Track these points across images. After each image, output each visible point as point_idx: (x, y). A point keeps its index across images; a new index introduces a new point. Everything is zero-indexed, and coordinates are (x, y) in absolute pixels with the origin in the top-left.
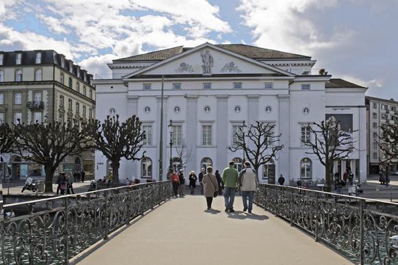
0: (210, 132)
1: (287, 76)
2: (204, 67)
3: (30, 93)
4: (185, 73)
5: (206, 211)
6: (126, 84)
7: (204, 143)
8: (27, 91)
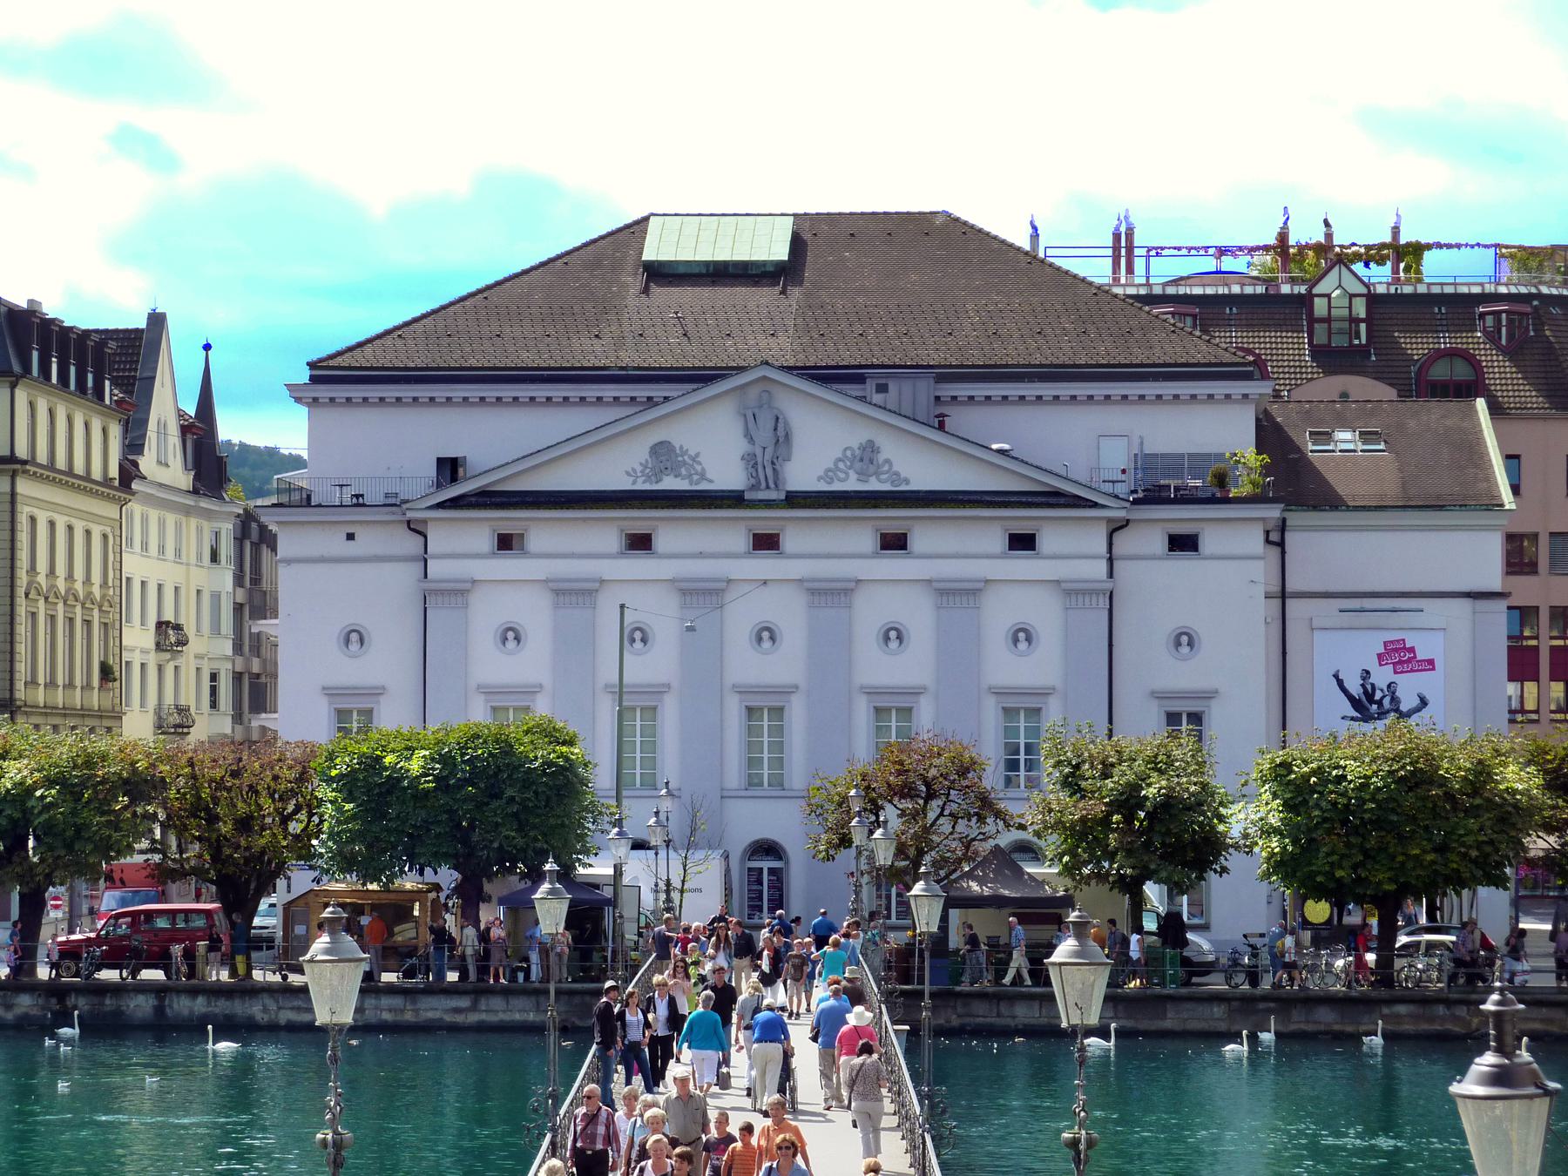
0: (778, 731)
1: (1095, 505)
2: (751, 461)
4: (670, 483)
5: (1338, 671)
6: (417, 529)
7: (753, 782)
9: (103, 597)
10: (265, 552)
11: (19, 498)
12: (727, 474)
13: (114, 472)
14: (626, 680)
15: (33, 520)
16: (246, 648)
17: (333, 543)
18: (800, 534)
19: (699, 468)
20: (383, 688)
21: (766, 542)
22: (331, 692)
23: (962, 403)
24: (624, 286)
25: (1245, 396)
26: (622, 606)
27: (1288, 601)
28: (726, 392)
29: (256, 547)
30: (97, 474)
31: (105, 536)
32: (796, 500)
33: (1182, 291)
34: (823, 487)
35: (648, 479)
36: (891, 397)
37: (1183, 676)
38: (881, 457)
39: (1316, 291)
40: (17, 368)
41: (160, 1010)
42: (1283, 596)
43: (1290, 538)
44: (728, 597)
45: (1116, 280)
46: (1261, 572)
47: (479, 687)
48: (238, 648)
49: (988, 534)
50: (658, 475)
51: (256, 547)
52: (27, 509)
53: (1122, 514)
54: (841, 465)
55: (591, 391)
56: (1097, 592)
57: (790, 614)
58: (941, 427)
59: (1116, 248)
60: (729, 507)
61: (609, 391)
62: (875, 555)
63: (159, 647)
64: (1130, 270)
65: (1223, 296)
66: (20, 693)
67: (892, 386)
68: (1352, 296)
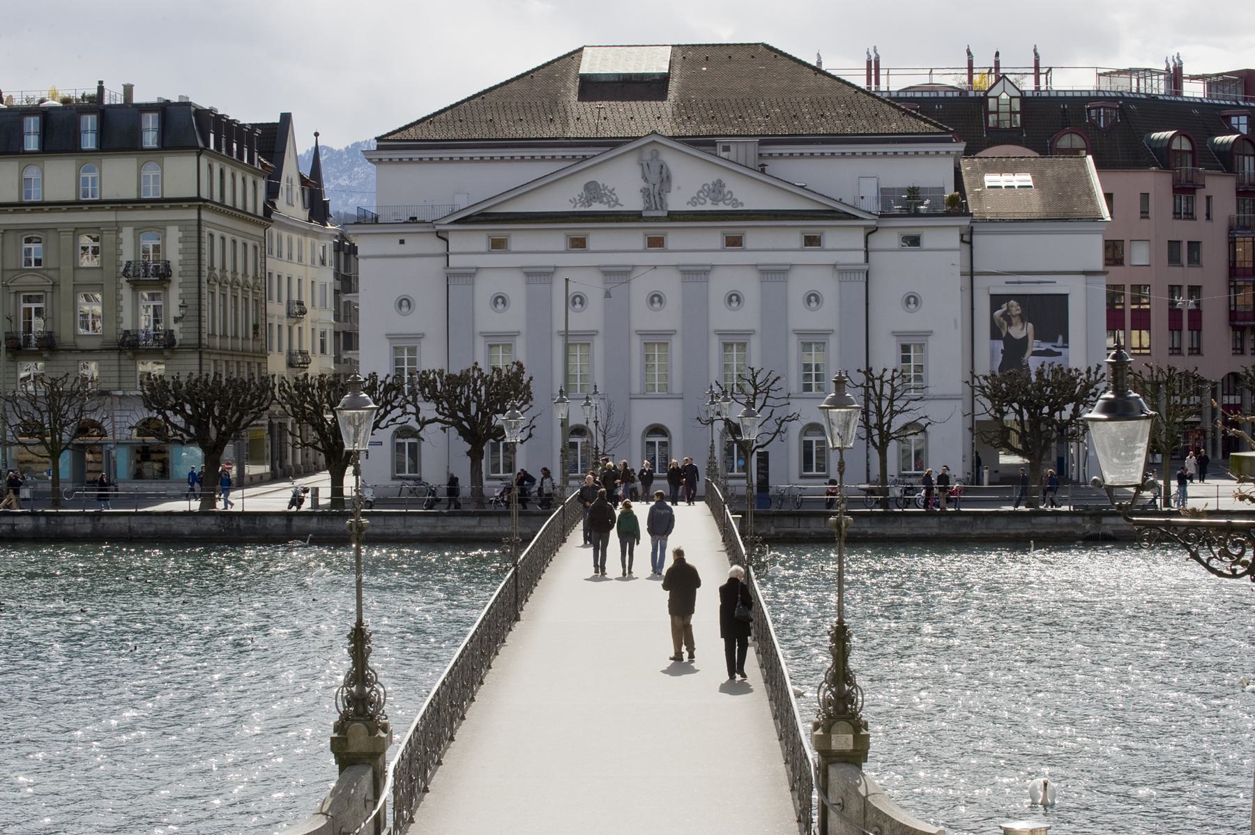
1: (856, 218)
2: (646, 193)
3: (127, 234)
4: (597, 207)
5: (664, 672)
6: (442, 236)
8: (117, 227)
9: (254, 284)
11: (203, 223)
12: (631, 201)
13: (260, 212)
14: (569, 329)
15: (211, 235)
16: (342, 318)
17: (391, 246)
18: (677, 239)
19: (614, 197)
20: (423, 334)
21: (656, 243)
22: (391, 337)
23: (776, 158)
24: (569, 90)
25: (948, 152)
26: (567, 280)
27: (975, 278)
28: (631, 151)
29: (347, 256)
30: (250, 209)
31: (255, 247)
32: (674, 216)
33: (909, 95)
34: (690, 208)
35: (583, 204)
36: (732, 154)
37: (912, 322)
38: (726, 190)
39: (989, 95)
40: (201, 145)
41: (289, 526)
42: (972, 274)
43: (977, 239)
44: (634, 275)
46: (957, 259)
47: (481, 333)
48: (337, 317)
49: (792, 237)
50: (589, 201)
52: (208, 229)
53: (874, 223)
54: (701, 195)
55: (548, 153)
56: (859, 271)
57: (671, 285)
58: (763, 171)
59: (869, 69)
60: (633, 221)
61: (559, 152)
62: (723, 250)
63: (289, 315)
64: (877, 82)
65: (934, 98)
66: (205, 341)
67: (733, 148)
68: (1011, 97)
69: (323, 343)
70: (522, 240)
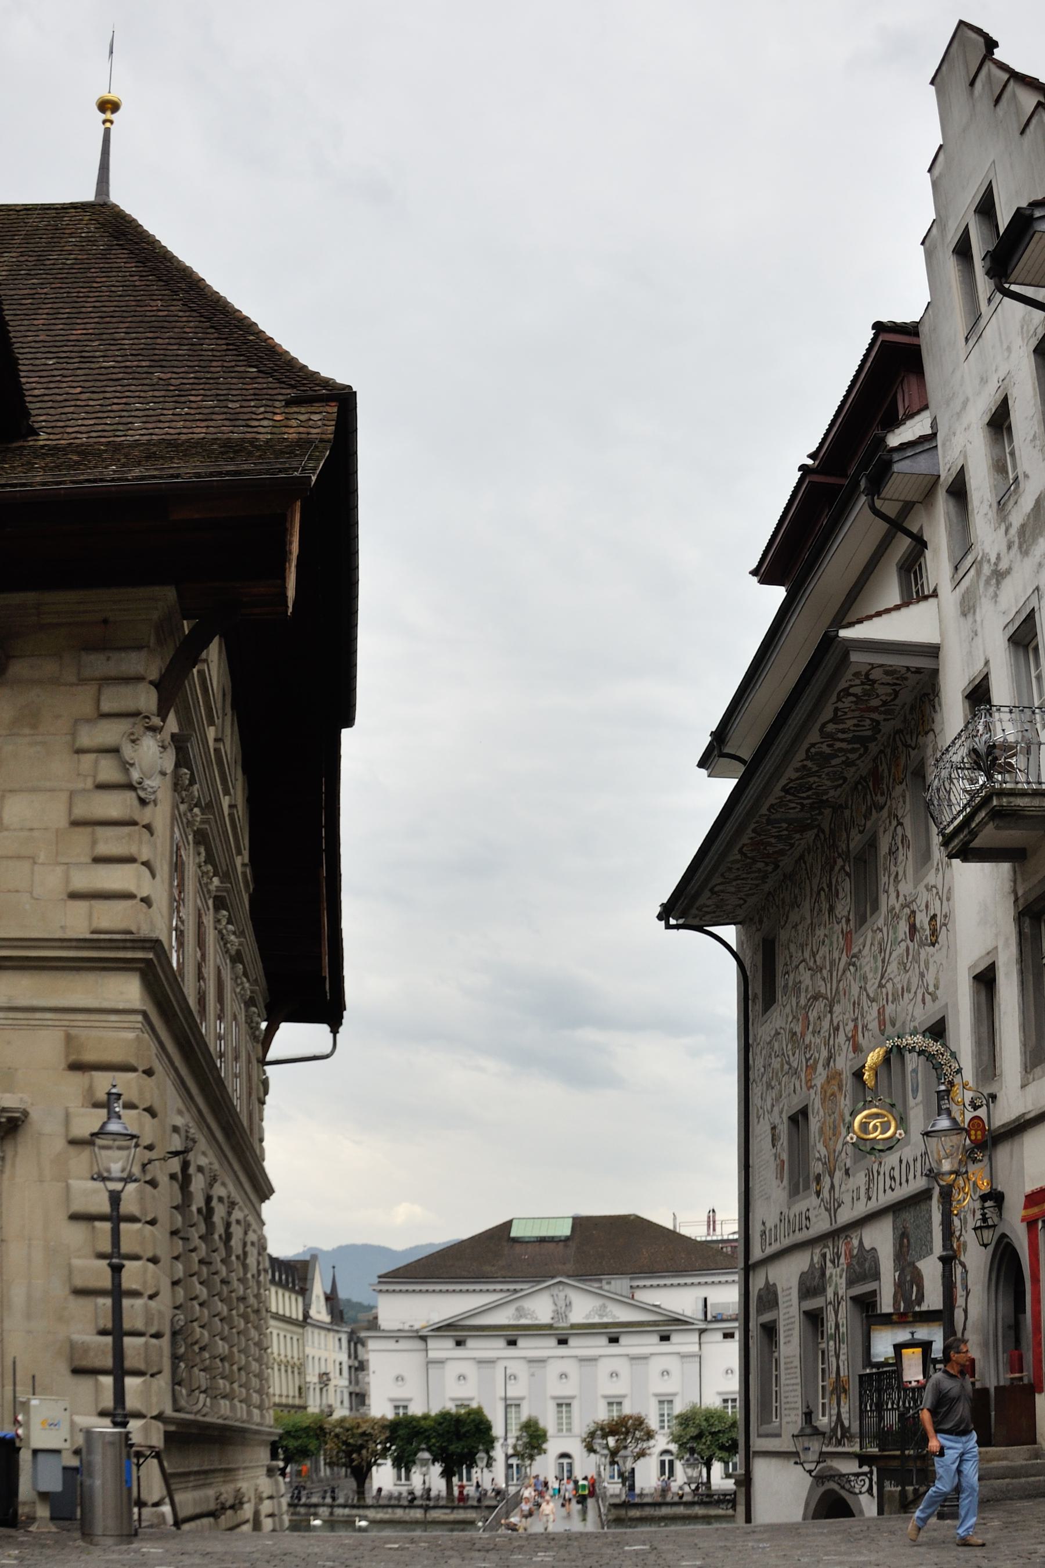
4: (523, 1321)
10: (359, 1347)
13: (301, 1318)
22: (392, 1400)
26: (506, 1368)
29: (356, 1344)
45: (709, 1234)
51: (356, 1344)
56: (695, 1356)
59: (709, 1222)
64: (714, 1230)
69: (341, 1370)
70: (478, 1348)
